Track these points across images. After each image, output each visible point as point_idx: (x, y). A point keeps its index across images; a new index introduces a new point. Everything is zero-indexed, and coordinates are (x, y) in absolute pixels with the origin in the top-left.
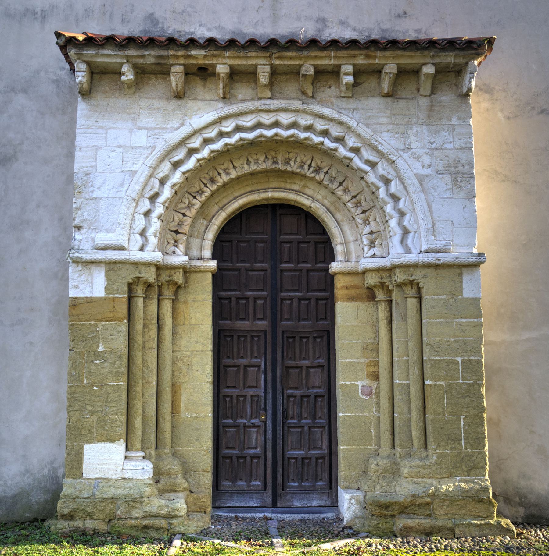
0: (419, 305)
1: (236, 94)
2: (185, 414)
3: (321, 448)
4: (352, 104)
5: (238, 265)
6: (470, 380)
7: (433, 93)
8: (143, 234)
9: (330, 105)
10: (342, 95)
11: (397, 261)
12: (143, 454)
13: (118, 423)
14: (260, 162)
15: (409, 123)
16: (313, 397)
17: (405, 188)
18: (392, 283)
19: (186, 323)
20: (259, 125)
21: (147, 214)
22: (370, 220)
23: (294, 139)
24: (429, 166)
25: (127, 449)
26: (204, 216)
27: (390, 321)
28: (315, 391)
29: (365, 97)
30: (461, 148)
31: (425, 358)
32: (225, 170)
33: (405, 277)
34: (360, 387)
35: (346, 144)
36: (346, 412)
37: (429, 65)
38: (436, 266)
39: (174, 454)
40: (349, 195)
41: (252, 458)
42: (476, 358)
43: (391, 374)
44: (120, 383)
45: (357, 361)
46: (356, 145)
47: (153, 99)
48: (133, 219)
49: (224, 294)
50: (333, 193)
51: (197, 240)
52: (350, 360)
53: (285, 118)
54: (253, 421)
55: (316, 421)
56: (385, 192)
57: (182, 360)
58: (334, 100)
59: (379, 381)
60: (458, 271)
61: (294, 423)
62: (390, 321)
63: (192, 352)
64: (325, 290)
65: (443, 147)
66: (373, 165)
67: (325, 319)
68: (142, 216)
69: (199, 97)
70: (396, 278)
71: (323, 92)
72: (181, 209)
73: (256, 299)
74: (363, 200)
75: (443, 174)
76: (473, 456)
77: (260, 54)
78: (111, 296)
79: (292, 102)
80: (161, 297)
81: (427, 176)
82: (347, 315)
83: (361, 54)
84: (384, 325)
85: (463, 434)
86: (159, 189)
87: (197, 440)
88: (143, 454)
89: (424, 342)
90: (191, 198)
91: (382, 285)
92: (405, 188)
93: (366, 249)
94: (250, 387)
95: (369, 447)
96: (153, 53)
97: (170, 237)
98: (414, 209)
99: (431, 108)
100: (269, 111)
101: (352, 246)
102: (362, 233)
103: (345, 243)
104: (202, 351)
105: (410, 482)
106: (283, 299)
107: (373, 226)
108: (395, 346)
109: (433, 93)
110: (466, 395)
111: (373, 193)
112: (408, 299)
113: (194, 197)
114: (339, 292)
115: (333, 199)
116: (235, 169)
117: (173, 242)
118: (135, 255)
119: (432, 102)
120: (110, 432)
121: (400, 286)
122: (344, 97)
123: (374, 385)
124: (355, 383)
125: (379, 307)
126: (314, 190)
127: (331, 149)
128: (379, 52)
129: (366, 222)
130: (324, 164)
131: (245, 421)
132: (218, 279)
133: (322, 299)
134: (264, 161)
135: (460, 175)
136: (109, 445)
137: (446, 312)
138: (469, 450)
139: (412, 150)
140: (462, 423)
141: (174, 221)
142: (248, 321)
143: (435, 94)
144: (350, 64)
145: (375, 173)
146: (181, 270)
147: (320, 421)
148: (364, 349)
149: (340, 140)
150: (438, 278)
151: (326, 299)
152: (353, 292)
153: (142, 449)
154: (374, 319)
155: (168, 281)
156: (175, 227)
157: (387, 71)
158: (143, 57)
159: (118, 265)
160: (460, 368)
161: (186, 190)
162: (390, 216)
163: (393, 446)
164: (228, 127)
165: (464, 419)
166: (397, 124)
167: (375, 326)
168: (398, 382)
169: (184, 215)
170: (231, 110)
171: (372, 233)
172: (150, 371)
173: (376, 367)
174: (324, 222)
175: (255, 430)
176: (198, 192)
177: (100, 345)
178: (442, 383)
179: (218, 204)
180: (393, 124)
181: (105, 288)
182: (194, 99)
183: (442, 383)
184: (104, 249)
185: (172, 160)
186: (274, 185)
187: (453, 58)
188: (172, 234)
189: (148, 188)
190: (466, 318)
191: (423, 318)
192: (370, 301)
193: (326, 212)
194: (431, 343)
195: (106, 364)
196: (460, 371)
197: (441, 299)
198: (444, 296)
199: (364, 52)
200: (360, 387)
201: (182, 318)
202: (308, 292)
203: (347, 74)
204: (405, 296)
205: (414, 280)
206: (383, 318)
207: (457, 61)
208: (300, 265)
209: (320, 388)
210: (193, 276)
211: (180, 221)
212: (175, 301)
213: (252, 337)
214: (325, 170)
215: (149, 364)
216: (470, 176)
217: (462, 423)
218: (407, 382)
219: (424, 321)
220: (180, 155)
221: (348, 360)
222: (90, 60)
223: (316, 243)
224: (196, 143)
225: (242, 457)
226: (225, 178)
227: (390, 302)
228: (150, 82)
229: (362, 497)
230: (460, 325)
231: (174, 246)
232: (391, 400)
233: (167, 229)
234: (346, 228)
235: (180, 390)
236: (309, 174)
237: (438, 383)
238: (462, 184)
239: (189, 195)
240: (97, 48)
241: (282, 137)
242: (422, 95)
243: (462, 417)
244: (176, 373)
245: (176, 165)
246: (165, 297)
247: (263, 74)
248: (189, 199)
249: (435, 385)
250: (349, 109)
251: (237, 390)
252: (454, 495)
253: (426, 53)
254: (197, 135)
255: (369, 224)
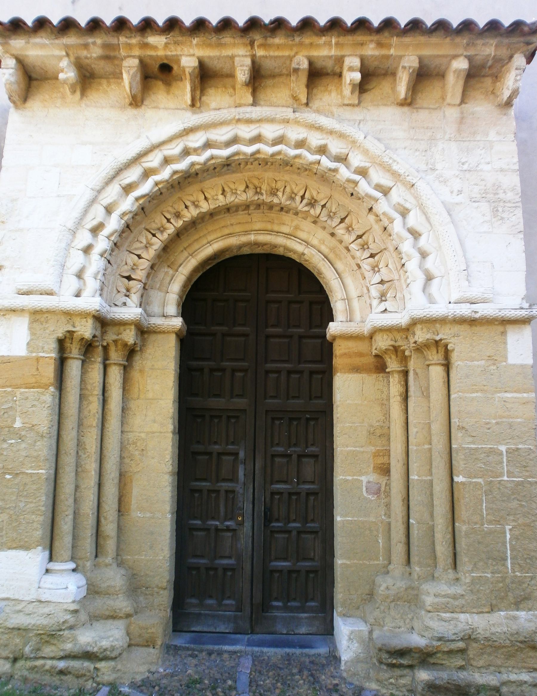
0: (445, 375)
1: (209, 102)
2: (136, 514)
3: (312, 560)
4: (357, 114)
5: (213, 328)
6: (519, 477)
7: (463, 101)
8: (79, 275)
9: (330, 114)
10: (346, 102)
11: (419, 313)
12: (72, 565)
13: (35, 525)
14: (239, 192)
15: (432, 139)
16: (303, 494)
17: (428, 219)
18: (409, 347)
19: (142, 396)
20: (235, 140)
21: (87, 250)
22: (380, 267)
23: (281, 157)
24: (460, 192)
25: (51, 559)
26: (169, 264)
27: (406, 398)
28: (307, 487)
29: (374, 105)
30: (502, 170)
31: (454, 446)
32: (193, 203)
33: (429, 336)
34: (364, 484)
35: (350, 165)
36: (346, 516)
37: (461, 59)
38: (471, 322)
39: (120, 564)
40: (352, 234)
41: (225, 570)
42: (527, 447)
43: (406, 466)
44: (41, 471)
45: (362, 449)
46: (363, 164)
47: (102, 107)
48: (66, 256)
49: (195, 364)
50: (333, 235)
51: (160, 293)
52: (352, 448)
53: (270, 131)
54: (228, 523)
55: (308, 525)
56: (401, 224)
57: (134, 443)
58: (334, 109)
59: (389, 476)
60: (500, 328)
61: (278, 526)
62: (406, 398)
63: (147, 433)
64: (321, 362)
65: (478, 169)
66: (386, 192)
67: (321, 397)
68: (81, 252)
69: (162, 106)
70: (416, 338)
71: (321, 99)
72: (136, 249)
73: (234, 371)
74: (371, 241)
75: (478, 202)
76: (524, 583)
77: (238, 41)
78: (34, 354)
79: (280, 109)
80: (108, 362)
81: (457, 204)
82: (349, 390)
83: (372, 41)
84: (397, 403)
85: (509, 552)
86: (105, 219)
87: (151, 548)
88: (72, 565)
89: (452, 424)
90: (150, 236)
91: (396, 349)
92: (428, 219)
93: (375, 302)
94: (224, 480)
95: (376, 562)
96: (99, 41)
97: (121, 284)
98: (440, 247)
99: (462, 120)
100: (249, 121)
101: (356, 304)
102: (370, 282)
103: (348, 299)
104: (161, 432)
105: (436, 619)
106: (267, 372)
107: (384, 274)
108: (412, 430)
109: (463, 101)
110: (513, 497)
111: (385, 229)
112: (430, 367)
113: (154, 235)
114: (337, 362)
115: (333, 242)
116: (207, 201)
117: (125, 291)
118: (66, 301)
119: (462, 113)
120: (24, 537)
121: (420, 349)
122: (347, 105)
123: (383, 481)
124: (359, 478)
125: (391, 380)
126: (309, 233)
127: (330, 170)
128: (395, 38)
129: (375, 269)
130: (321, 196)
131: (217, 523)
132: (187, 344)
133: (317, 372)
134: (245, 191)
135: (502, 204)
136: (22, 554)
137: (485, 383)
138: (518, 574)
139: (437, 172)
140: (508, 536)
141: (126, 264)
142: (224, 398)
143: (466, 103)
144: (356, 55)
145: (388, 200)
146: (133, 327)
147: (312, 525)
148: (371, 433)
149: (342, 159)
150: (474, 338)
151: (323, 372)
152: (357, 361)
153: (73, 559)
154: (384, 396)
155: (115, 341)
156: (127, 271)
157: (406, 65)
158: (86, 46)
159: (46, 315)
160: (505, 460)
161: (143, 226)
162: (408, 256)
163: (408, 561)
164: (197, 141)
165: (510, 530)
166: (417, 140)
167: (384, 405)
168: (416, 477)
169: (139, 257)
170: (201, 120)
171: (382, 282)
172: (88, 456)
173: (386, 458)
174: (320, 273)
175: (229, 534)
176: (159, 229)
177: (18, 419)
178: (480, 480)
179: (188, 249)
180: (412, 139)
181: (28, 344)
182: (154, 108)
183: (480, 480)
184: (27, 293)
185: (123, 182)
186: (258, 226)
187: (493, 49)
188: (116, 277)
189: (90, 216)
190: (512, 392)
191: (451, 393)
192: (379, 373)
193: (323, 260)
194: (464, 425)
195: (23, 445)
196: (505, 464)
197: (478, 366)
198: (483, 362)
199: (375, 38)
200: (364, 484)
201: (136, 390)
202: (299, 363)
203: (351, 69)
204: (428, 363)
205: (441, 340)
206: (397, 394)
207: (499, 53)
208: (290, 330)
209: (313, 483)
210: (153, 337)
211: (134, 265)
212: (126, 369)
213: (229, 417)
214: (323, 203)
215: (88, 447)
216: (514, 205)
217: (508, 536)
218: (429, 478)
219: (453, 396)
220: (133, 175)
221: (349, 449)
222: (19, 53)
223: (311, 303)
224: (154, 160)
225: (211, 569)
226: (194, 212)
227: (406, 373)
228: (101, 88)
229: (367, 633)
230: (505, 401)
231: (126, 296)
232: (406, 502)
233: (117, 274)
234: (349, 281)
235: (132, 482)
236: (302, 207)
237: (474, 480)
238: (505, 215)
239: (148, 233)
240: (27, 36)
241: (266, 155)
242: (449, 105)
243: (508, 527)
244: (127, 461)
245: (128, 189)
246: (112, 362)
247: (242, 68)
248: (146, 237)
249: (471, 483)
250: (355, 120)
251: (208, 484)
252: (499, 638)
253: (458, 40)
254: (156, 151)
255: (379, 271)
